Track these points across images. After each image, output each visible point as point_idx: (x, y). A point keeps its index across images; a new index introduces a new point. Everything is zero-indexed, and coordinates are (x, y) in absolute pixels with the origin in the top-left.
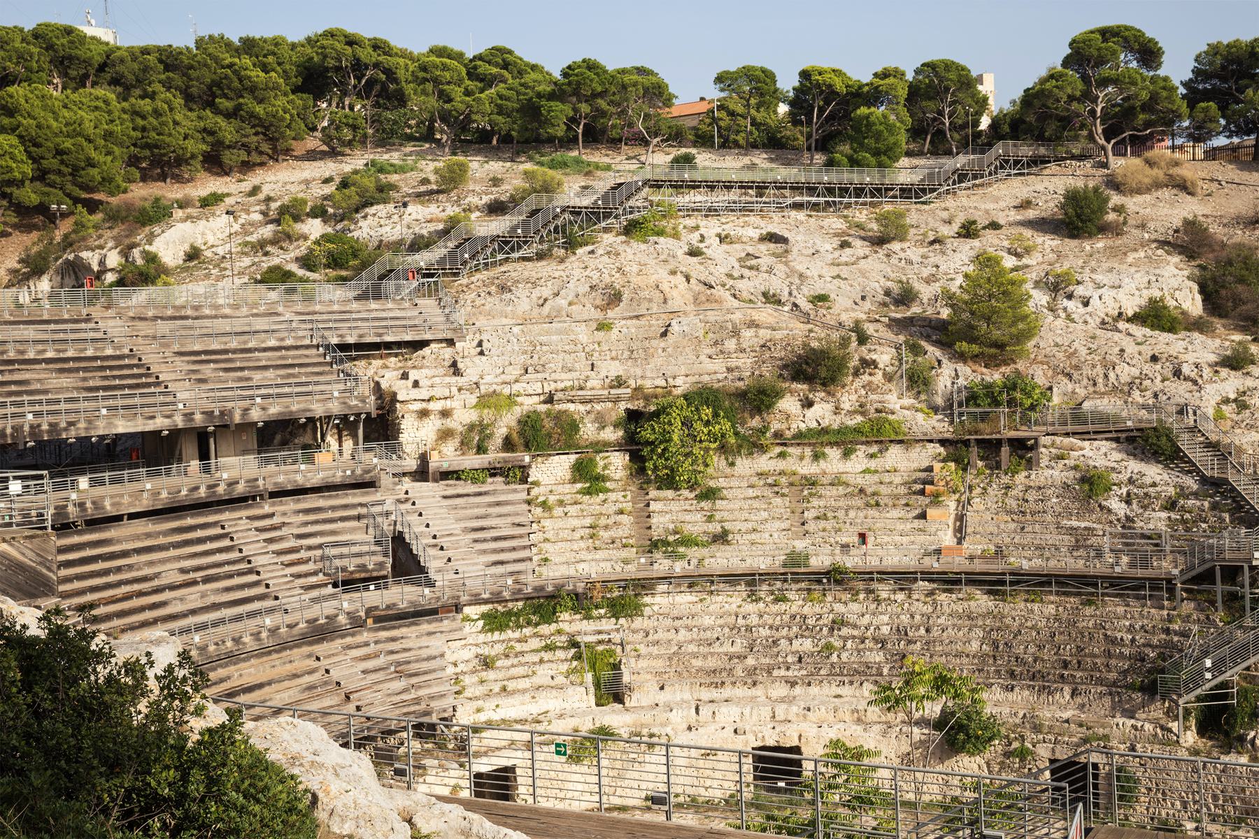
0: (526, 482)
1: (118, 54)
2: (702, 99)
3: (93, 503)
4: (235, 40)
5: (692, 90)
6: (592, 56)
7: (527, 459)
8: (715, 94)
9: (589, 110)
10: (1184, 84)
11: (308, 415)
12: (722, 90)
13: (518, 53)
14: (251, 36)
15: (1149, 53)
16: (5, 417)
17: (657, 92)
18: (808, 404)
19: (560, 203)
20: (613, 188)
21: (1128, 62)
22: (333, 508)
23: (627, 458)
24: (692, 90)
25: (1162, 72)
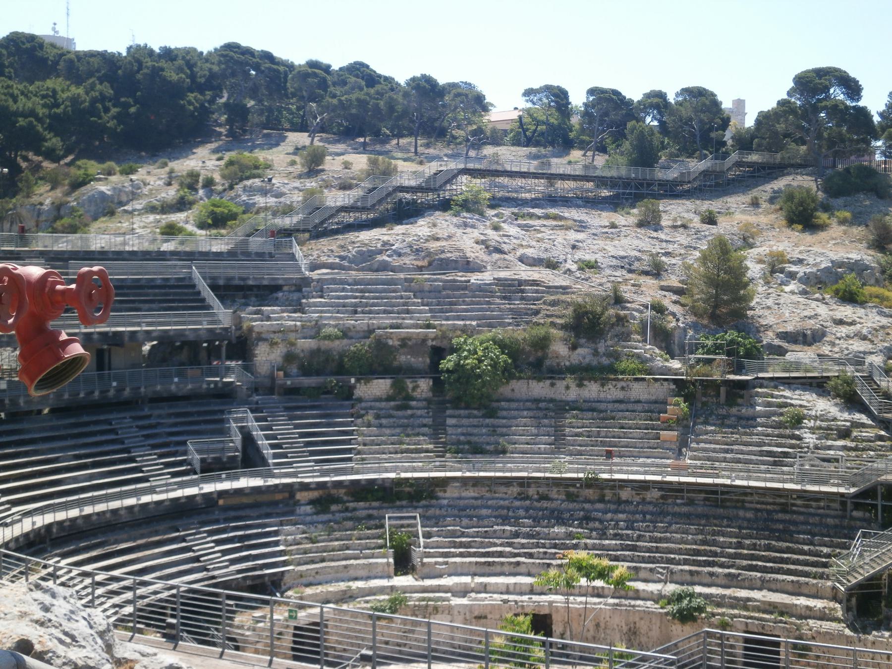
1: (68, 56)
2: (516, 108)
3: (10, 400)
4: (157, 50)
5: (506, 105)
6: (315, 57)
7: (353, 380)
8: (523, 104)
9: (433, 111)
10: (881, 115)
11: (183, 339)
13: (372, 67)
15: (853, 88)
16: (887, 645)
17: (479, 103)
21: (837, 94)
22: (199, 413)
23: (431, 383)
24: (506, 105)
25: (861, 104)
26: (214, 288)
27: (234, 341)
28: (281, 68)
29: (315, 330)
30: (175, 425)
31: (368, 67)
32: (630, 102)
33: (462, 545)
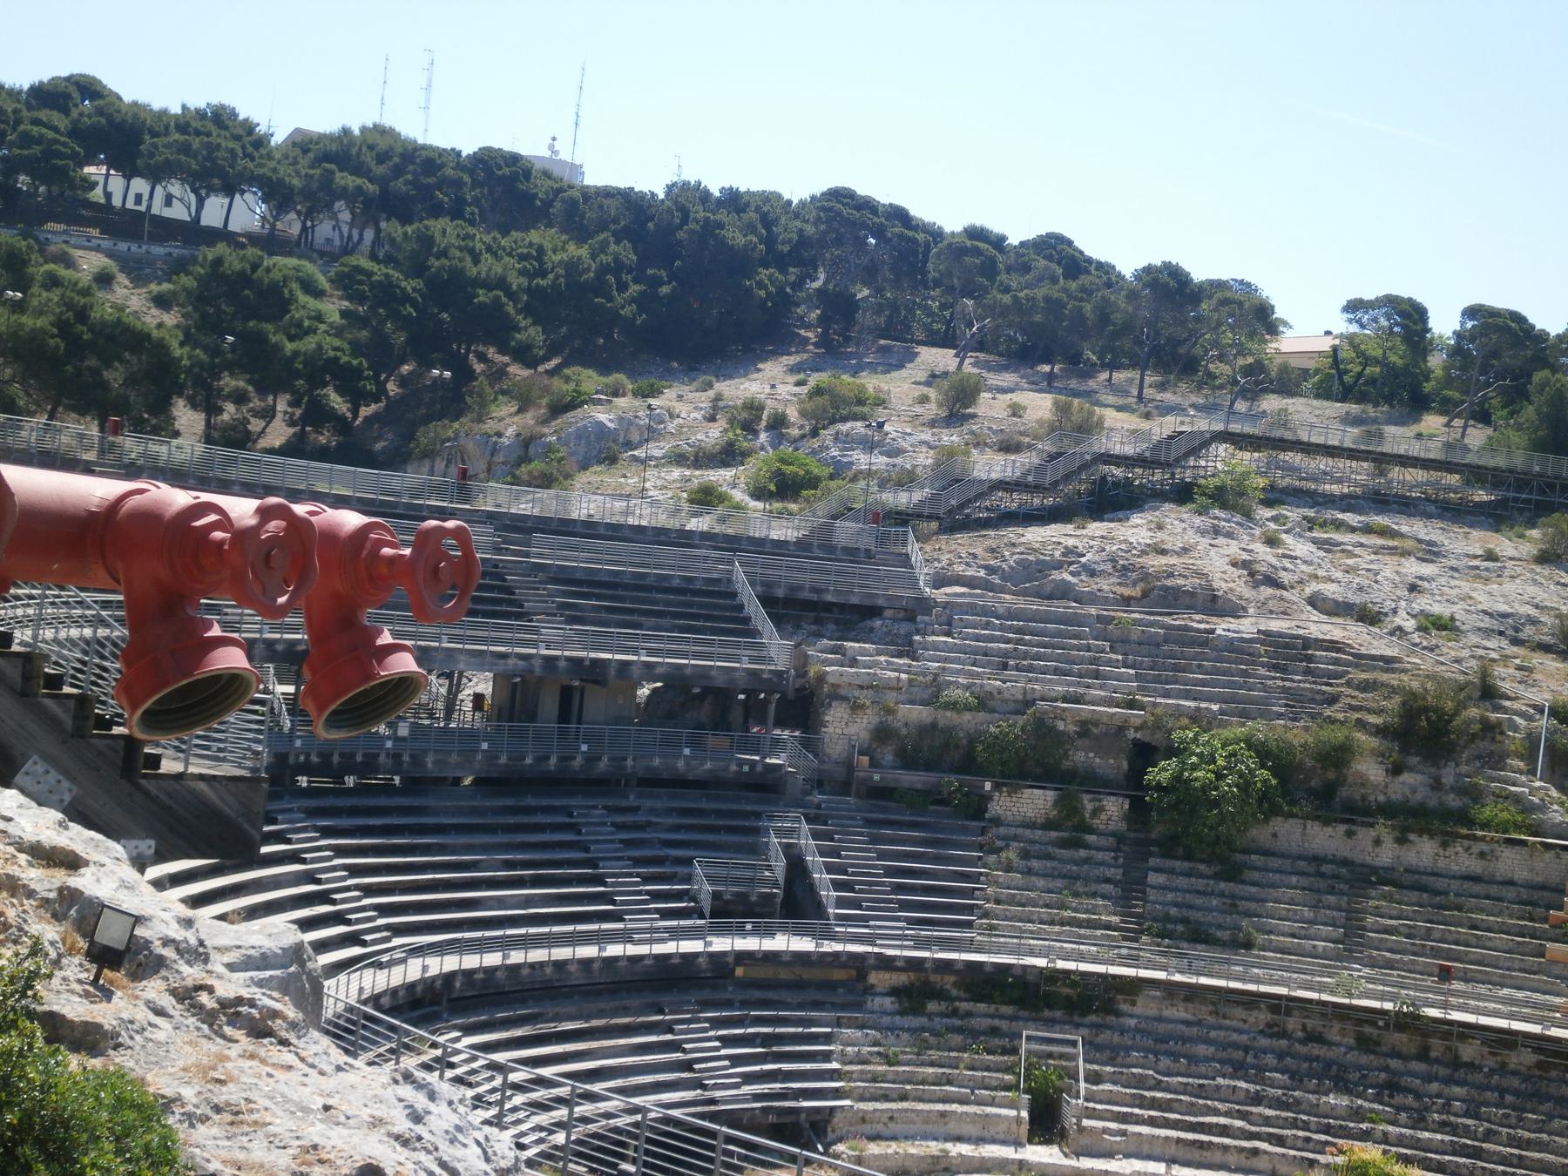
0: (983, 819)
2: (1328, 333)
3: (412, 756)
5: (1310, 322)
7: (988, 786)
8: (1342, 325)
9: (1182, 327)
11: (706, 683)
12: (1350, 321)
14: (978, 224)
17: (1262, 318)
18: (1396, 770)
19: (1096, 448)
20: (1170, 437)
22: (720, 814)
24: (1310, 322)
26: (767, 601)
27: (791, 696)
28: (921, 237)
29: (933, 692)
30: (677, 828)
31: (1070, 243)
32: (1543, 336)
33: (1154, 1104)
